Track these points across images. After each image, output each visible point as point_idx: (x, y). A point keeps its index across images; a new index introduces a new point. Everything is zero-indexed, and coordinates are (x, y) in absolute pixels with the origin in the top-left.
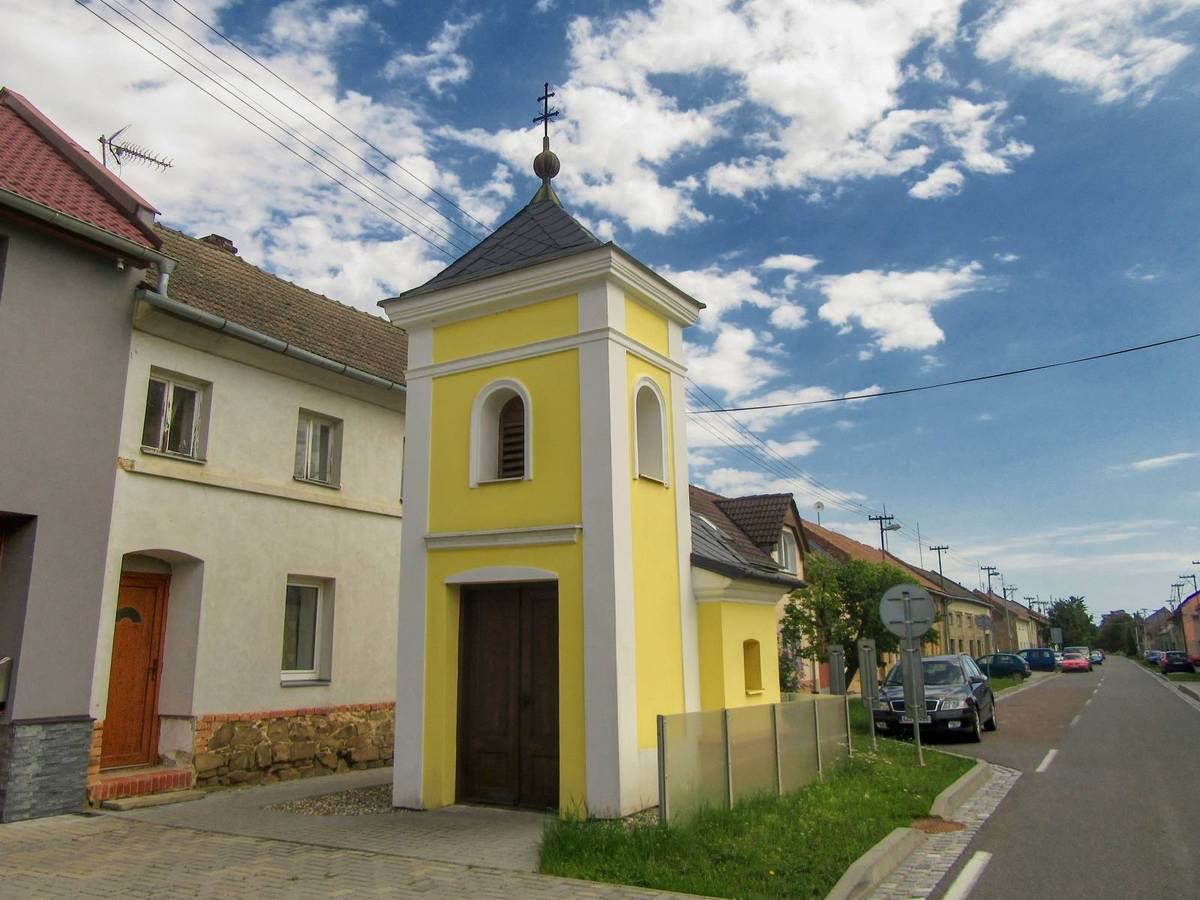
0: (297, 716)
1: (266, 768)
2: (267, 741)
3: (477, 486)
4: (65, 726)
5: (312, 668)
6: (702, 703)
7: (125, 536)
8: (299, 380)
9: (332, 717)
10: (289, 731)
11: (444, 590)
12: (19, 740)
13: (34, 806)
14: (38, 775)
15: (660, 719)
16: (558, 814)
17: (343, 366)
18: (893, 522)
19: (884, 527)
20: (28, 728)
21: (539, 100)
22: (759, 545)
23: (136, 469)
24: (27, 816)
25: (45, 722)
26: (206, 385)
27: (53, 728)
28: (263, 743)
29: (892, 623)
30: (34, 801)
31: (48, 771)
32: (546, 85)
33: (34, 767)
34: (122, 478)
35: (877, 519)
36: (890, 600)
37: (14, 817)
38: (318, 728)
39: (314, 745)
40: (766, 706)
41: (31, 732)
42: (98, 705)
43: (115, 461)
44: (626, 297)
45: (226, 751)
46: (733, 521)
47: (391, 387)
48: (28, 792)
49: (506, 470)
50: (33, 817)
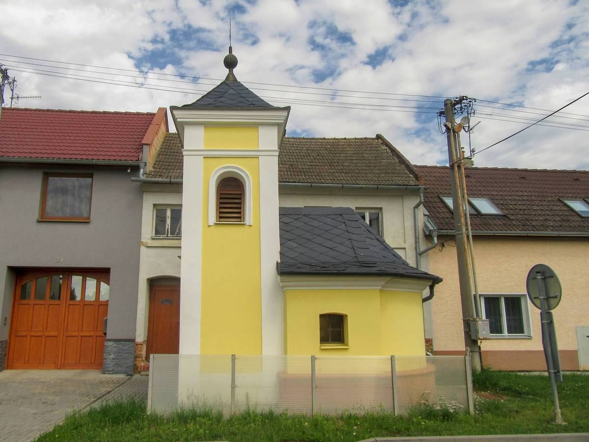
4: (122, 342)
6: (559, 351)
7: (146, 272)
8: (374, 196)
12: (106, 346)
13: (113, 370)
14: (114, 359)
20: (109, 342)
23: (148, 246)
24: (111, 373)
25: (116, 341)
26: (381, 209)
27: (119, 343)
30: (113, 368)
31: (118, 358)
33: (112, 356)
34: (143, 249)
37: (106, 373)
41: (111, 343)
42: (140, 336)
43: (140, 243)
47: (311, 186)
48: (110, 364)
49: (221, 217)
50: (113, 374)
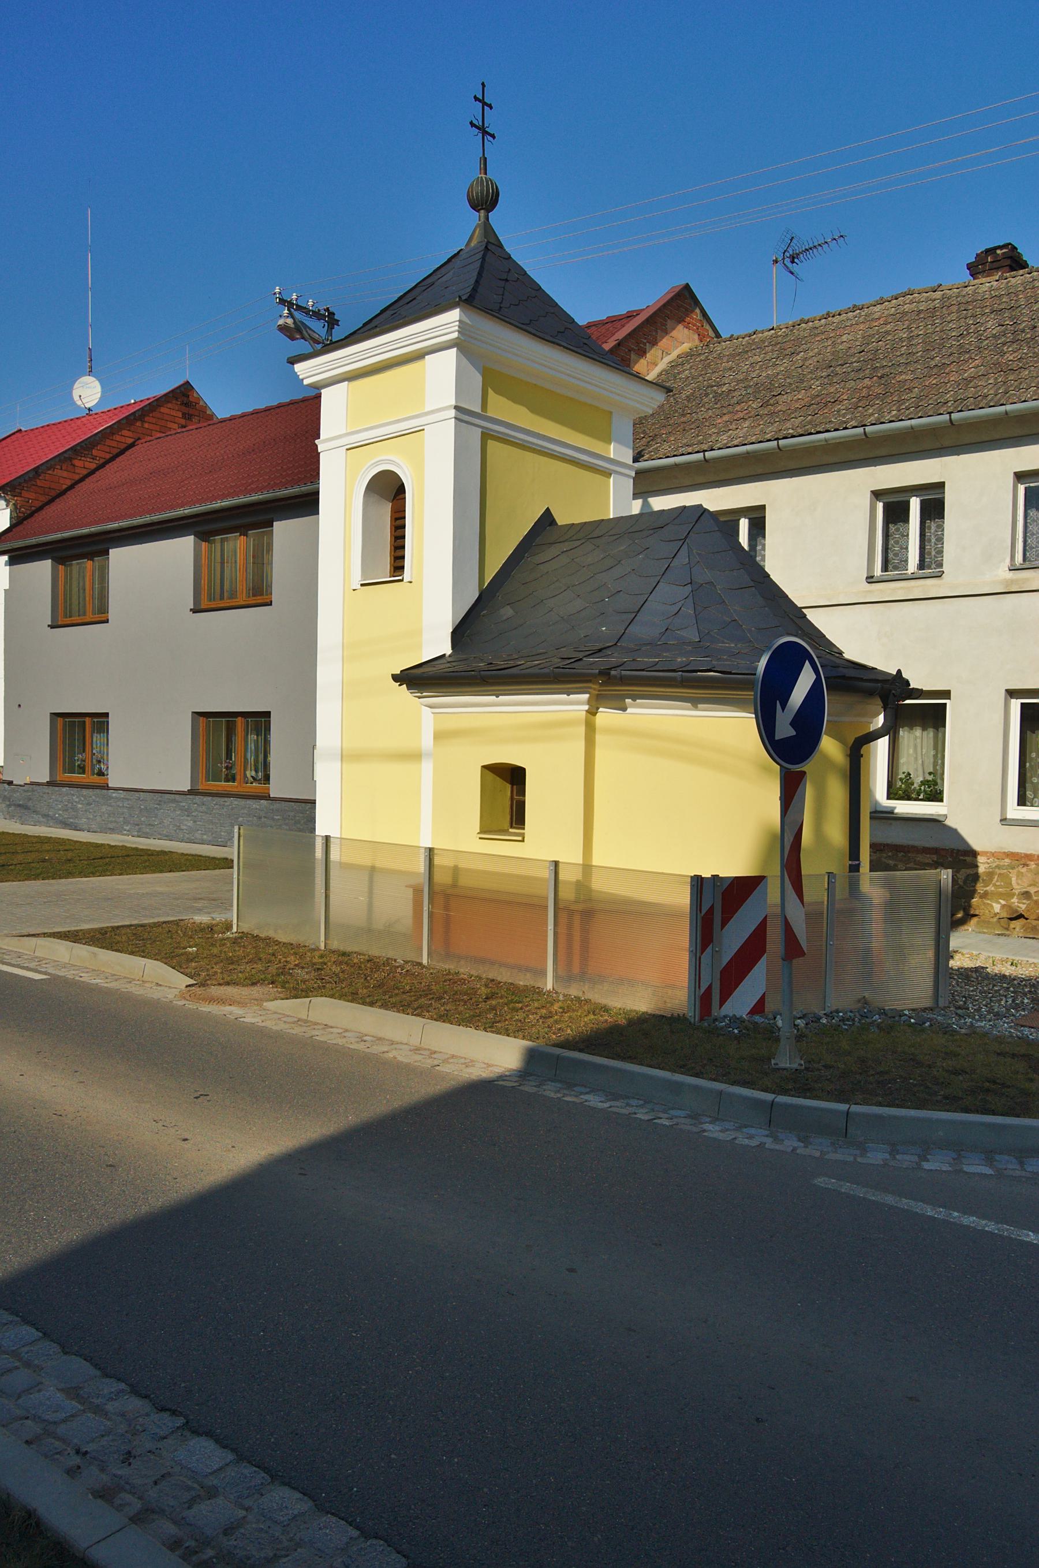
17: (861, 430)
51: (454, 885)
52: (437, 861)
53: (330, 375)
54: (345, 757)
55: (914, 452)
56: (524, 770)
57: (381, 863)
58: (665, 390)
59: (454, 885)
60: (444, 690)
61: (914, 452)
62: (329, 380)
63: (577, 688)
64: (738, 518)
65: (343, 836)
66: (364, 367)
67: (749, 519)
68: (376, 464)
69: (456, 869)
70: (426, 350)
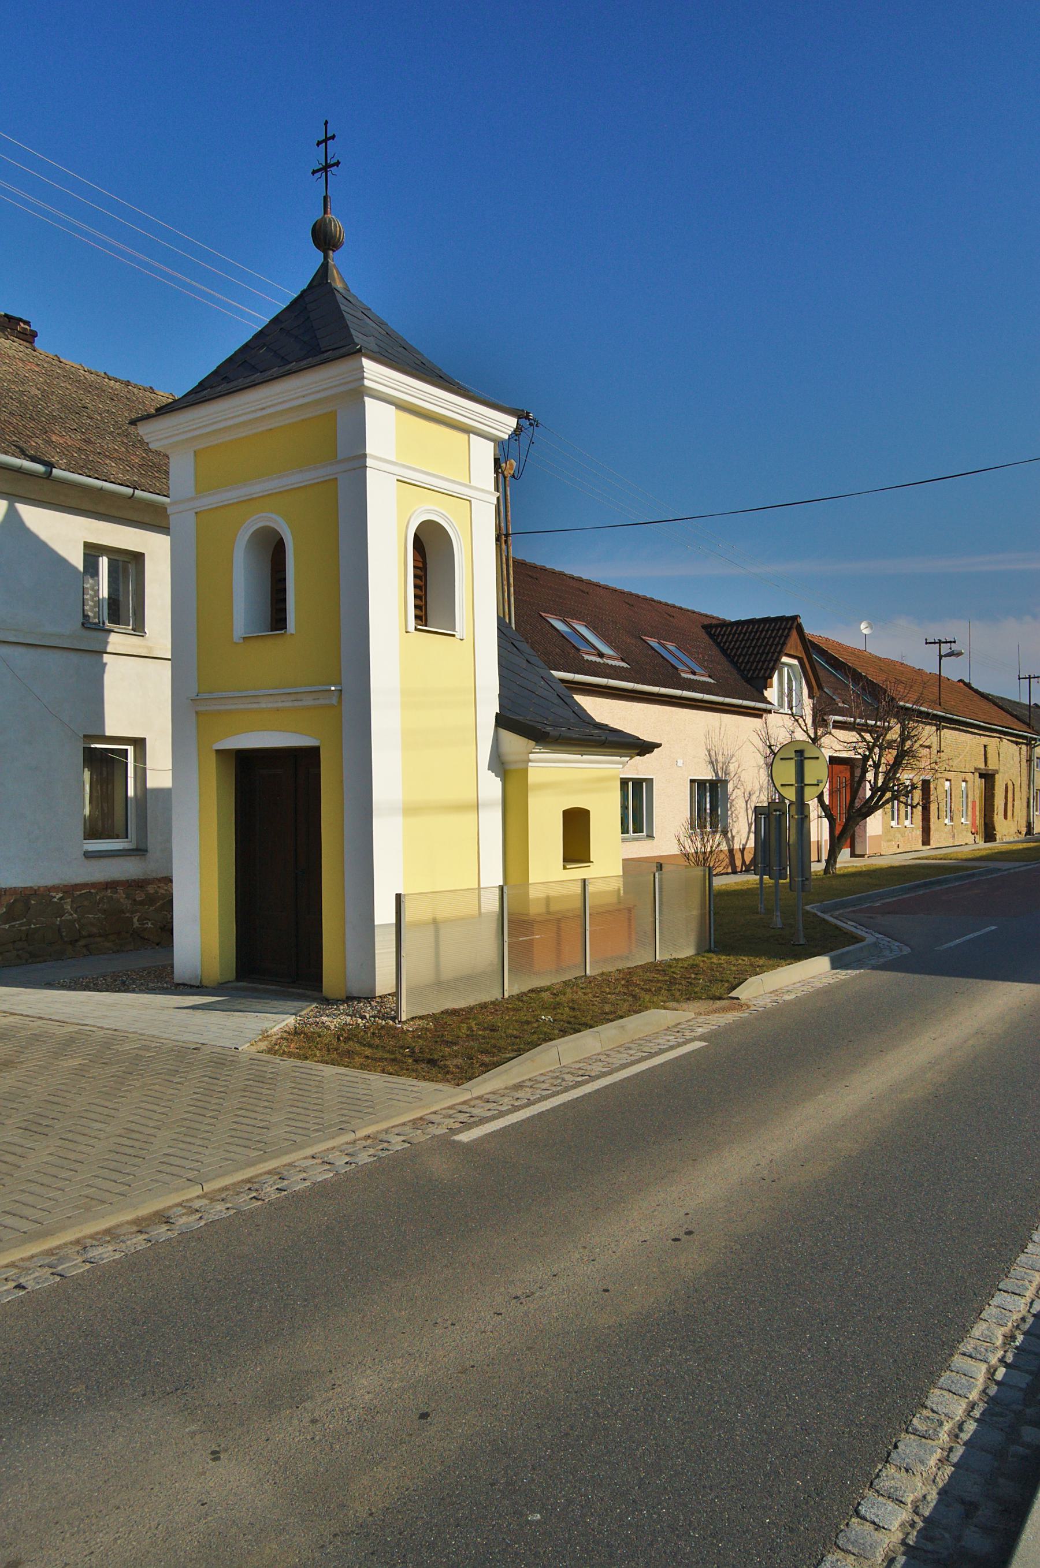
0: (106, 889)
1: (73, 942)
2: (71, 915)
3: (241, 641)
5: (127, 838)
9: (151, 889)
10: (99, 904)
11: (213, 757)
15: (398, 897)
16: (322, 991)
17: (131, 491)
18: (954, 647)
19: (942, 654)
21: (333, 137)
22: (748, 681)
28: (66, 917)
29: (782, 785)
32: (326, 123)
35: (935, 643)
36: (782, 759)
38: (135, 900)
39: (131, 919)
40: (170, 869)
44: (396, 408)
45: (21, 925)
46: (724, 651)
51: (548, 912)
52: (590, 889)
53: (437, 411)
54: (411, 810)
55: (28, 498)
56: (588, 812)
57: (442, 913)
58: (955, 652)
59: (548, 912)
60: (554, 748)
61: (28, 498)
62: (383, 395)
63: (612, 752)
64: (97, 554)
65: (482, 892)
66: (437, 413)
67: (109, 559)
68: (429, 511)
69: (548, 900)
70: (475, 430)
